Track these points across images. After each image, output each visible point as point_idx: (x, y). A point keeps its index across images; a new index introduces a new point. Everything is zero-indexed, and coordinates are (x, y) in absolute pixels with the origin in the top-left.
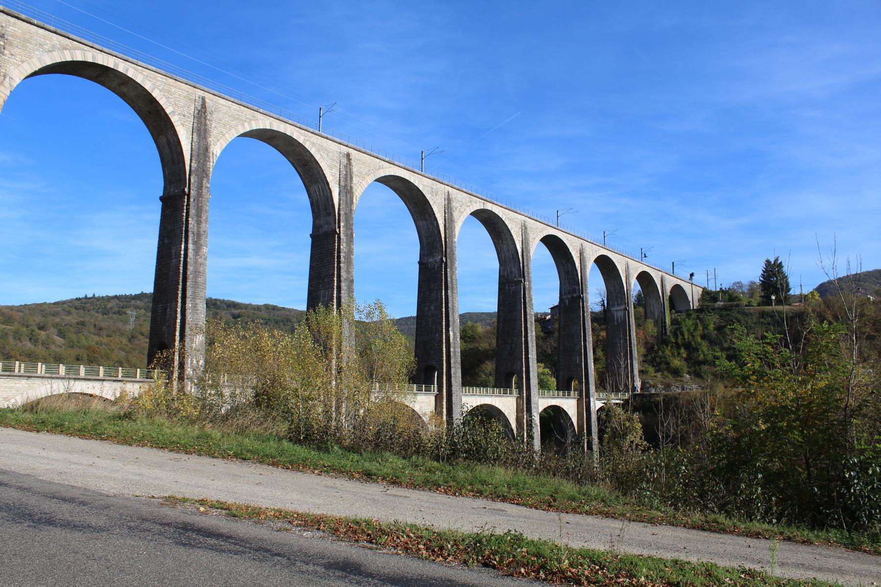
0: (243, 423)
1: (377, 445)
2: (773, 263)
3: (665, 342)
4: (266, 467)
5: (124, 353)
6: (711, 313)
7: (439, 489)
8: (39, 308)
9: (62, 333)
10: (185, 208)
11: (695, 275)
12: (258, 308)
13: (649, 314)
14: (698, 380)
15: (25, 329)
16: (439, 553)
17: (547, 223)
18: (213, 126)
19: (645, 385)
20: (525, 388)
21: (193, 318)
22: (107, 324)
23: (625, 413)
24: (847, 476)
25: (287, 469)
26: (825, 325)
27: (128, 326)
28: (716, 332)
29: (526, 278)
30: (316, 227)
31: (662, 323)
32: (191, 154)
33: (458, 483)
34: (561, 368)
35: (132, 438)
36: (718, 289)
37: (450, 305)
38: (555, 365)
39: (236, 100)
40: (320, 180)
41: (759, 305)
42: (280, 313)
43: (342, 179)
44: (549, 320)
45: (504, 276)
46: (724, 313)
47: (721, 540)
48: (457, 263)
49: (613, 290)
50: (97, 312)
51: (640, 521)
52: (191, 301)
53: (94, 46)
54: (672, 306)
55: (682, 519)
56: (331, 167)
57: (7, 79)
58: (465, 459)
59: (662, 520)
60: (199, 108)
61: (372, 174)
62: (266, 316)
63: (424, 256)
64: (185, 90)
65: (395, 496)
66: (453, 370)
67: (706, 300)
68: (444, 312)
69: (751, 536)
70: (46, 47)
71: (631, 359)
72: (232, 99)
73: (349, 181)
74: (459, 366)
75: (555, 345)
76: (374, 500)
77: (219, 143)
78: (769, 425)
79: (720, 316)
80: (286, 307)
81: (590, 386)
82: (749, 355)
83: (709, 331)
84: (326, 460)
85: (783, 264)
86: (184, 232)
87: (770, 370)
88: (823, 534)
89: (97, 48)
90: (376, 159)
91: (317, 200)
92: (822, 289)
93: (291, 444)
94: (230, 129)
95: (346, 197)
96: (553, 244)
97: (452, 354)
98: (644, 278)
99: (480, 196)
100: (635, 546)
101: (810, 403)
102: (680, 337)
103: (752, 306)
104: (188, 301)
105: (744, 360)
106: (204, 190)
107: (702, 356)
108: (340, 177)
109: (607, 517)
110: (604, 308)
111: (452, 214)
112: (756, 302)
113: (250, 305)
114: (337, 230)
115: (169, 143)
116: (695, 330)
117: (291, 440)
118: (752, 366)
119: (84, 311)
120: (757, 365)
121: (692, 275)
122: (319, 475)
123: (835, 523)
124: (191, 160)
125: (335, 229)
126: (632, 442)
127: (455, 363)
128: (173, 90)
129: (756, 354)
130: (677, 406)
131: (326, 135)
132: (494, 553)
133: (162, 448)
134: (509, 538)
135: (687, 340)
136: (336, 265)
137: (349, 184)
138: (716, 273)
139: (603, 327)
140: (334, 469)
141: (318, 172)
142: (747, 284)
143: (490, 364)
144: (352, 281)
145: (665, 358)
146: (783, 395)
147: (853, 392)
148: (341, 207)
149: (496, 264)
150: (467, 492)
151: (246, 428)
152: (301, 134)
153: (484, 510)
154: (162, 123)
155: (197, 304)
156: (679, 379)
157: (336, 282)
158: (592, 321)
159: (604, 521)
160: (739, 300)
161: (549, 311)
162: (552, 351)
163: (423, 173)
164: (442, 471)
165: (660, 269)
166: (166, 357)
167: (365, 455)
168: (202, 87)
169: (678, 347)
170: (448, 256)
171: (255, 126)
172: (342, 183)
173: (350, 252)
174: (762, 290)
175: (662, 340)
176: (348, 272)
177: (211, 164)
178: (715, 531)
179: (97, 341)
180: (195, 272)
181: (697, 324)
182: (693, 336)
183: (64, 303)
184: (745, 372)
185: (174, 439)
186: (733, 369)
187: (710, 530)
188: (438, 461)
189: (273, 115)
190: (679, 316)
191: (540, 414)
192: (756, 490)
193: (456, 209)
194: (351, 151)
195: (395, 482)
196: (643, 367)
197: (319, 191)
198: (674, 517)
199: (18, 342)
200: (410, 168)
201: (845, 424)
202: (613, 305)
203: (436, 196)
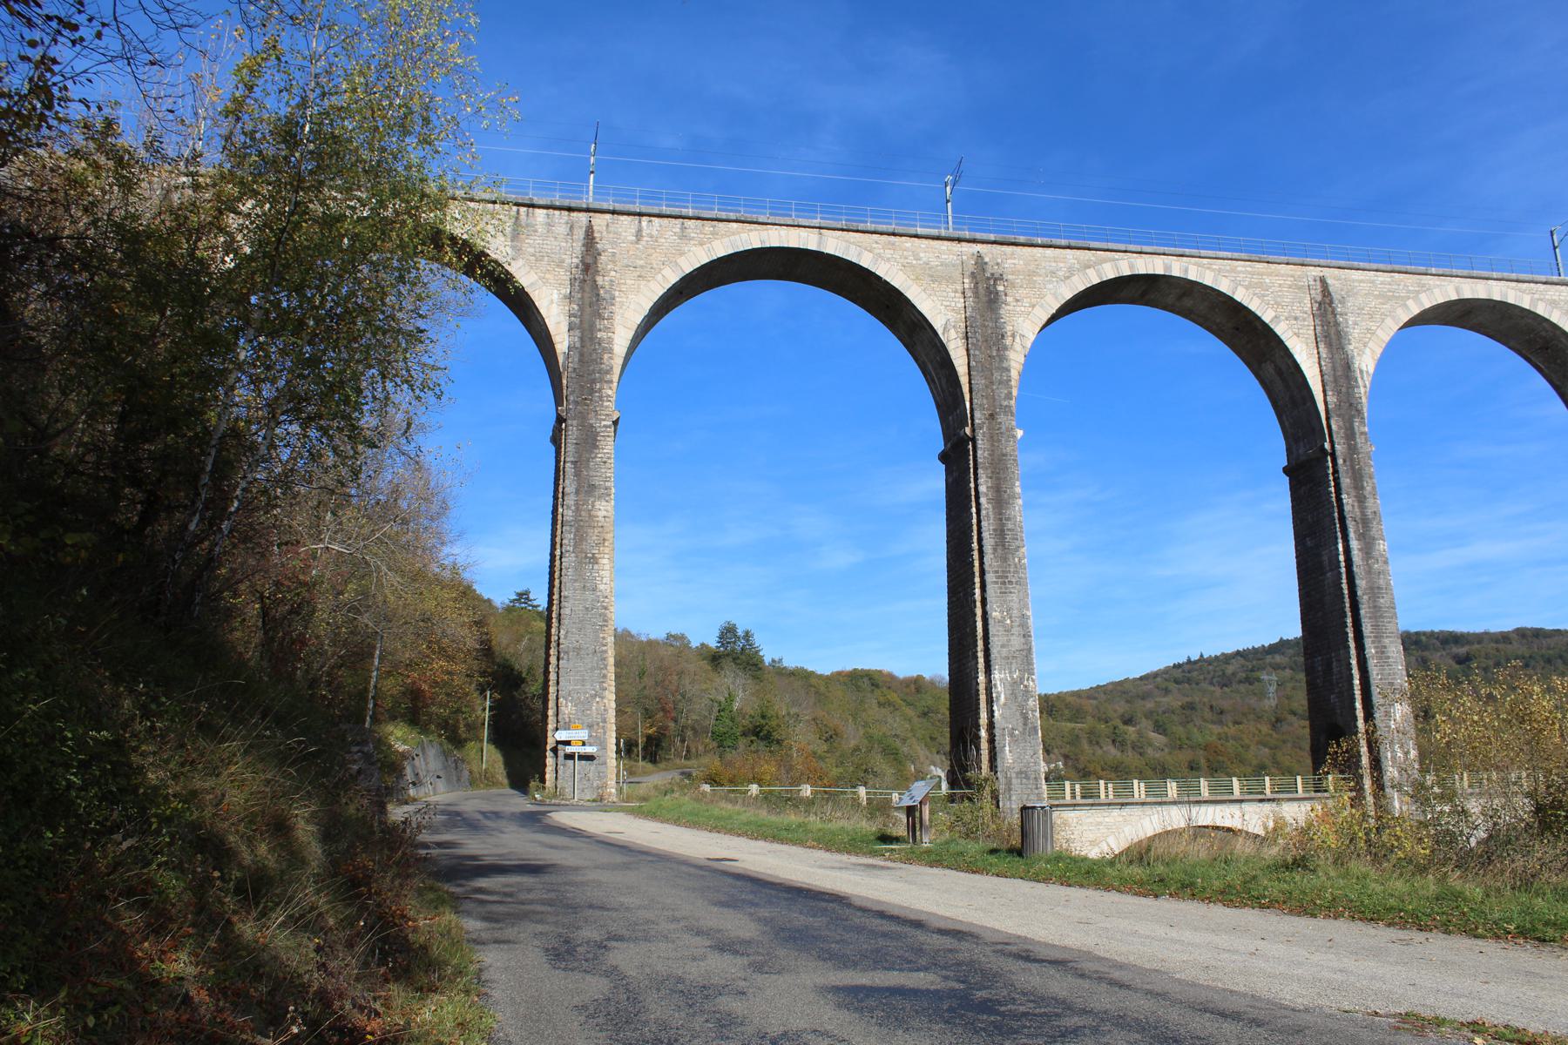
0: (1525, 867)
5: (1267, 750)
8: (1119, 688)
10: (1331, 478)
21: (1382, 674)
27: (1266, 701)
32: (1322, 381)
35: (1315, 904)
39: (1382, 266)
50: (1211, 683)
52: (1373, 642)
57: (1018, 339)
60: (1319, 298)
62: (1524, 650)
64: (1288, 276)
72: (1375, 266)
77: (1367, 351)
86: (1337, 521)
89: (1134, 250)
94: (1383, 320)
104: (1368, 643)
106: (1358, 440)
113: (1486, 633)
115: (1279, 372)
124: (1324, 391)
128: (1267, 281)
133: (1372, 919)
152: (1524, 292)
154: (1262, 341)
155: (1385, 647)
166: (1347, 751)
168: (1316, 261)
171: (1427, 303)
177: (1363, 390)
179: (1219, 734)
183: (1155, 675)
185: (1392, 902)
189: (1459, 272)
199: (1096, 748)
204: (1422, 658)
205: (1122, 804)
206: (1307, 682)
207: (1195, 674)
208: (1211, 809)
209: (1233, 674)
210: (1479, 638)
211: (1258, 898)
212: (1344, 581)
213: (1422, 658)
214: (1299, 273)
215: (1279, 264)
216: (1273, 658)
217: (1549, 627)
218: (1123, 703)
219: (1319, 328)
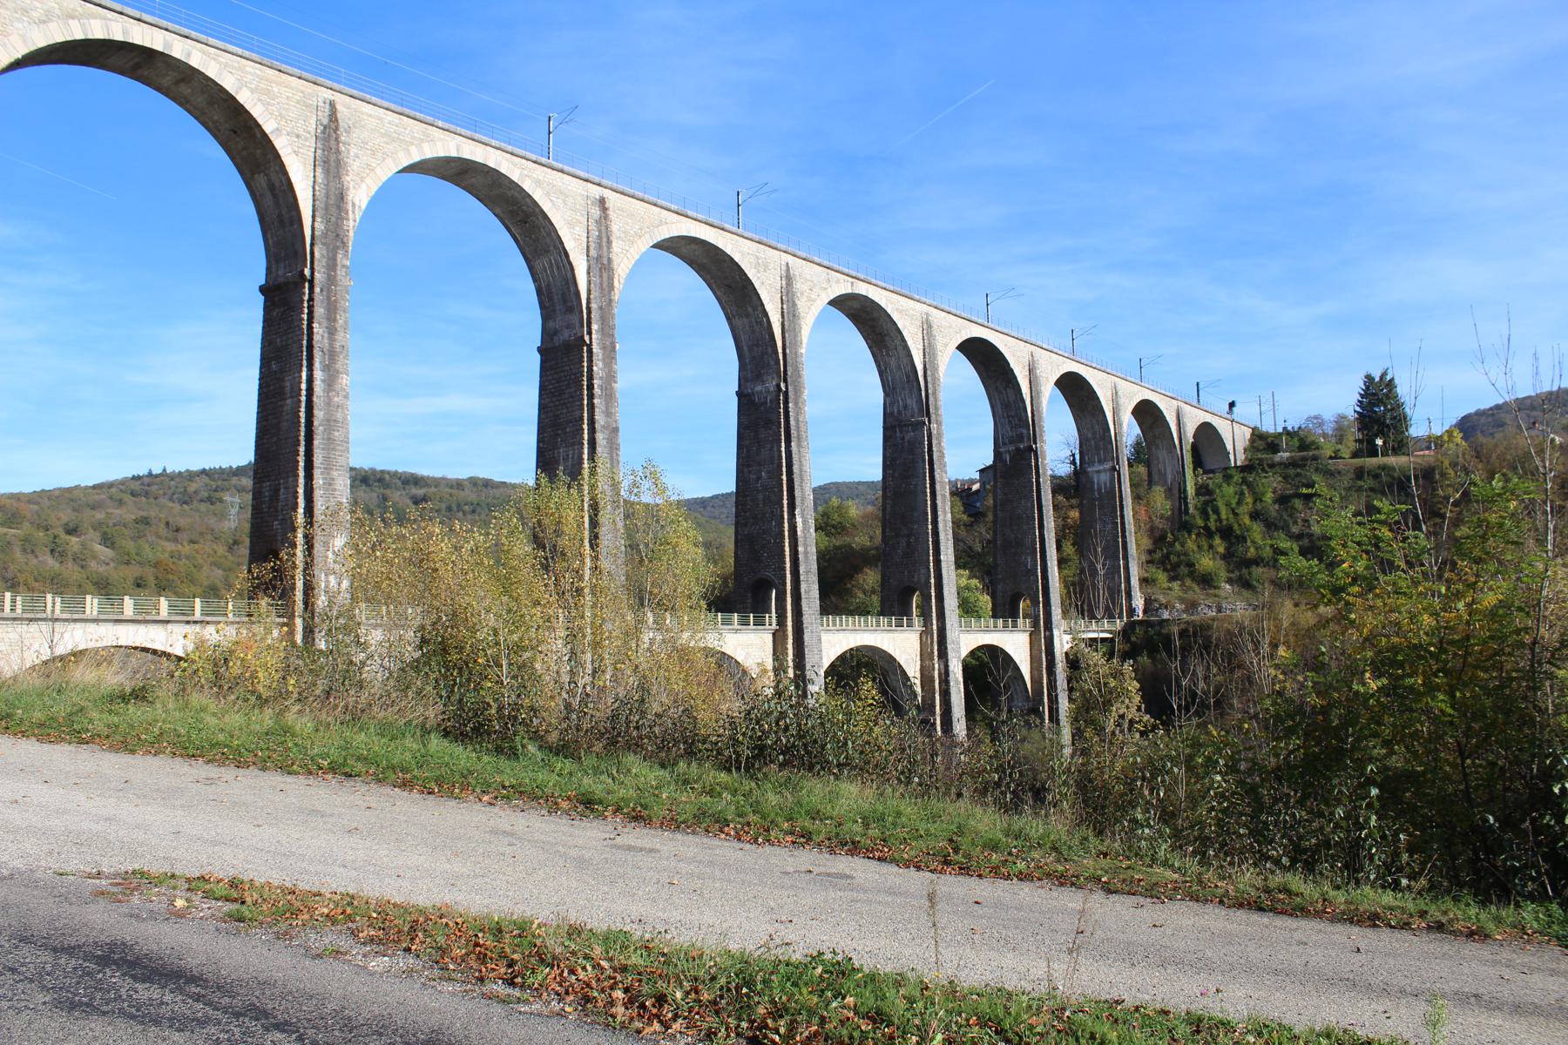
1: (613, 742)
2: (1377, 379)
3: (1186, 527)
4: (387, 790)
5: (220, 572)
6: (1267, 472)
7: (726, 829)
8: (67, 495)
9: (109, 539)
10: (306, 305)
11: (1237, 404)
12: (458, 484)
13: (1156, 477)
14: (1246, 593)
15: (41, 534)
16: (655, 1011)
17: (969, 317)
18: (352, 154)
19: (1151, 604)
20: (934, 615)
22: (189, 520)
23: (1107, 661)
24: (1556, 790)
25: (429, 793)
26: (1497, 483)
27: (226, 522)
28: (1277, 507)
29: (933, 417)
30: (547, 334)
31: (1180, 493)
32: (314, 206)
33: (764, 817)
34: (1000, 576)
36: (1280, 430)
37: (796, 468)
38: (989, 573)
39: (393, 107)
40: (552, 248)
41: (1355, 455)
42: (497, 492)
43: (592, 245)
44: (977, 492)
45: (892, 413)
46: (1291, 471)
47: (1297, 935)
48: (806, 391)
49: (1090, 435)
50: (171, 499)
51: (1129, 893)
52: (322, 473)
53: (125, 11)
54: (1198, 462)
55: (1216, 886)
56: (571, 225)
58: (782, 766)
59: (1175, 889)
60: (325, 121)
61: (647, 236)
62: (473, 498)
63: (747, 380)
64: (298, 90)
65: (630, 848)
66: (803, 587)
67: (1258, 450)
68: (785, 482)
69: (1359, 923)
70: (34, 14)
71: (1126, 558)
72: (386, 104)
73: (605, 248)
74: (815, 579)
75: (988, 536)
76: (581, 863)
77: (363, 186)
78: (1385, 681)
79: (1284, 478)
80: (508, 481)
81: (1053, 608)
82: (1344, 546)
83: (1264, 505)
84: (509, 771)
85: (1397, 381)
86: (305, 349)
87: (1384, 573)
88: (1508, 913)
89: (131, 14)
90: (654, 208)
91: (548, 286)
92: (1467, 425)
93: (446, 743)
94: (384, 159)
95: (601, 276)
96: (981, 354)
97: (801, 557)
98: (1146, 413)
99: (846, 271)
100: (1115, 960)
101: (1468, 638)
102: (1213, 517)
103: (1341, 458)
104: (317, 473)
105: (1336, 556)
106: (338, 272)
107: (1252, 550)
108: (588, 242)
109: (1062, 885)
110: (1076, 467)
111: (794, 304)
112: (1348, 451)
113: (443, 479)
114: (587, 338)
115: (272, 187)
116: (1239, 503)
117: (446, 734)
118: (1351, 567)
119: (148, 498)
120: (1360, 566)
121: (1232, 405)
122: (491, 804)
123: (1530, 886)
124: (314, 217)
125: (583, 336)
126: (1122, 717)
127: (807, 572)
128: (275, 89)
129: (1359, 544)
130: (1207, 640)
131: (560, 166)
132: (778, 1012)
133: (193, 756)
134: (820, 970)
135: (1225, 523)
136: (585, 402)
137: (605, 254)
138: (1276, 399)
139: (1074, 501)
140: (521, 792)
141: (549, 234)
142: (1332, 419)
143: (872, 573)
144: (616, 430)
145: (1186, 554)
146: (1413, 623)
147: (1547, 613)
148: (592, 296)
149: (878, 396)
150: (781, 836)
151: (363, 711)
152: (515, 165)
153: (808, 876)
154: (259, 151)
155: (333, 479)
156: (1212, 591)
157: (586, 431)
158: (1054, 492)
159: (1055, 894)
160: (1317, 448)
161: (977, 476)
162: (983, 548)
163: (740, 231)
164: (734, 792)
165: (1174, 396)
166: (258, 578)
167: (590, 761)
168: (329, 83)
169: (1209, 534)
170: (789, 380)
172: (593, 253)
173: (611, 377)
174: (1359, 430)
175: (1181, 522)
176: (608, 414)
177: (352, 223)
178: (1283, 912)
179: (172, 552)
180: (328, 420)
181: (1242, 494)
182: (1236, 515)
183: (111, 485)
184: (1337, 579)
185: (221, 737)
186: (1314, 574)
187: (1273, 910)
188: (729, 770)
189: (463, 131)
190: (1211, 479)
191: (964, 661)
192: (1367, 820)
193: (802, 294)
194: (607, 193)
195: (639, 817)
196: (1147, 572)
197: (551, 266)
198: (1200, 882)
200: (716, 222)
201: (1533, 678)
202: (1092, 463)
203: (765, 271)
204: (383, 495)
205: (31, 620)
206: (253, 506)
207: (154, 488)
208: (132, 628)
209: (195, 492)
210: (436, 482)
211: (79, 732)
212: (303, 409)
213: (383, 495)
214: (310, 91)
215: (291, 75)
216: (239, 480)
217: (497, 478)
218: (69, 511)
219: (319, 152)
